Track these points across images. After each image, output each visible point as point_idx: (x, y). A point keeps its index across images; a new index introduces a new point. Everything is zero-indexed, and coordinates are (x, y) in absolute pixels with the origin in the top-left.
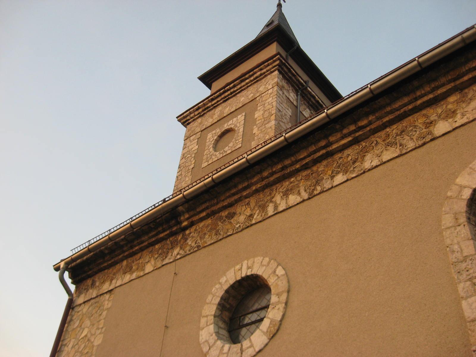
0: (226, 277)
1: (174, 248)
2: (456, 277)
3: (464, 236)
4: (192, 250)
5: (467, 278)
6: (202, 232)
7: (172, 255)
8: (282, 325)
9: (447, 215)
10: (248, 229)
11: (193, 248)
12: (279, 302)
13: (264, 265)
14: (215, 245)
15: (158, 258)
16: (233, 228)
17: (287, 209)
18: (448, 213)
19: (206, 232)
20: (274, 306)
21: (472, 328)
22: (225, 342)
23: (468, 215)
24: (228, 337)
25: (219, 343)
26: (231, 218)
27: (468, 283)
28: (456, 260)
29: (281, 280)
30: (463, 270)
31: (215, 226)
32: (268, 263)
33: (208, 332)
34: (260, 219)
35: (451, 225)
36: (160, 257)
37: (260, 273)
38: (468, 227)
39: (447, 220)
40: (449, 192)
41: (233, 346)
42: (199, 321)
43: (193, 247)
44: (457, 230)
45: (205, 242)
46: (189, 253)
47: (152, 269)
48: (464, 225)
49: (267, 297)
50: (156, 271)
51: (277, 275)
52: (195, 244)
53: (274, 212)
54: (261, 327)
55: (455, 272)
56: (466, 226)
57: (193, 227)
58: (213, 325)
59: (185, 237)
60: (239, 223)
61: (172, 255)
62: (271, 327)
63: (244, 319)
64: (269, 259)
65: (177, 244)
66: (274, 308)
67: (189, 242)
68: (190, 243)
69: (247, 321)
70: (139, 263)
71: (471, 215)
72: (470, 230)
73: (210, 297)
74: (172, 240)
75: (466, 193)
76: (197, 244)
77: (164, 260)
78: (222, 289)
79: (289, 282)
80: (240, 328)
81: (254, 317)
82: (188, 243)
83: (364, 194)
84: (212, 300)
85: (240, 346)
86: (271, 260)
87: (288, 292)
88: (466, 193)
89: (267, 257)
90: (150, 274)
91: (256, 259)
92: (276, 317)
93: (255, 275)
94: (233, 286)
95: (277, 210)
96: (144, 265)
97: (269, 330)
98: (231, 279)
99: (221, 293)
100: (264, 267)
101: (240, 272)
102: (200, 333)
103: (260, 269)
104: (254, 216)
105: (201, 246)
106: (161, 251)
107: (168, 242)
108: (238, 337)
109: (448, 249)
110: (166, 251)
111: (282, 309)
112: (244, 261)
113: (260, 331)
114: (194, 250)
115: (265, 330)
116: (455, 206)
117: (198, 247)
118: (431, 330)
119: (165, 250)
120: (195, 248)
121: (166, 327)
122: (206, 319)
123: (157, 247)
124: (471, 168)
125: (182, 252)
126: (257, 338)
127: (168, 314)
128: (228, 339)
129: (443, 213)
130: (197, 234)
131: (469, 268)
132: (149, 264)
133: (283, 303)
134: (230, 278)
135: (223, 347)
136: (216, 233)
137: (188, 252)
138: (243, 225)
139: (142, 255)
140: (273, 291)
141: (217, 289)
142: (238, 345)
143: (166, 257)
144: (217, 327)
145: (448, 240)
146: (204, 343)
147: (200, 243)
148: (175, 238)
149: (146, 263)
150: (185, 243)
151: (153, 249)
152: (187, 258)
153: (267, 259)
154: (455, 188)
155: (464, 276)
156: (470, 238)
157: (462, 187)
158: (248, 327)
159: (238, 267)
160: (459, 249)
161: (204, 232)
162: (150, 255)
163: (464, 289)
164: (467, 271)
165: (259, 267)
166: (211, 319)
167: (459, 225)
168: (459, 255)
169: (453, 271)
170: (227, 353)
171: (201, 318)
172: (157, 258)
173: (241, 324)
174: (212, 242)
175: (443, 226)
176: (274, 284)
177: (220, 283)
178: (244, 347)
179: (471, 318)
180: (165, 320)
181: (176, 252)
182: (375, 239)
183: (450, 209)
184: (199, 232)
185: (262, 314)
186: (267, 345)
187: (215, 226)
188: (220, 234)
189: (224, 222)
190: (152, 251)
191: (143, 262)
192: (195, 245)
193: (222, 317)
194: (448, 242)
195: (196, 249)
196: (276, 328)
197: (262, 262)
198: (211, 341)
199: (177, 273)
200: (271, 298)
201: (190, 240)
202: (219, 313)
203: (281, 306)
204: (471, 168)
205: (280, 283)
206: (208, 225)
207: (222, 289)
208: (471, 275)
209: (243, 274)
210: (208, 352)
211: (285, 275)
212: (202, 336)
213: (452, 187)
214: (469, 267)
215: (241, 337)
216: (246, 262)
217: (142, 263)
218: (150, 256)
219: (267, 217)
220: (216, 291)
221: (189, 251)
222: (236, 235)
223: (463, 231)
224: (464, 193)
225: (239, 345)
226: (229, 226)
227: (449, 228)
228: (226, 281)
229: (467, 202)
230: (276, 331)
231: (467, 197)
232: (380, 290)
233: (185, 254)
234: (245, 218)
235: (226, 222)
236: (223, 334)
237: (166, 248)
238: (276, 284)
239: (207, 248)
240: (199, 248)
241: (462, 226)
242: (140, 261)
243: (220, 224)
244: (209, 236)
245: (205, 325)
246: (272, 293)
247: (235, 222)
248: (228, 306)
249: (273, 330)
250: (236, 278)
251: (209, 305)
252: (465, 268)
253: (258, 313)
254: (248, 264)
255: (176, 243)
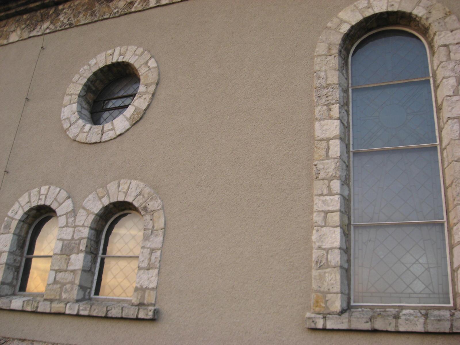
0: (96, 60)
1: (44, 21)
2: (316, 100)
3: (332, 66)
4: (63, 27)
5: (325, 103)
6: (77, 10)
7: (40, 28)
8: (145, 115)
9: (322, 44)
10: (126, 16)
11: (65, 25)
12: (146, 93)
13: (137, 55)
14: (89, 25)
15: (26, 29)
16: (111, 12)
17: (170, 4)
18: (323, 42)
19: (81, 11)
20: (141, 96)
21: (318, 146)
22: (87, 122)
23: (340, 48)
24: (89, 118)
25: (81, 122)
26: (110, 1)
27: (325, 108)
28: (318, 85)
29: (152, 72)
30: (323, 96)
31: (92, 6)
32: (142, 53)
33: (70, 110)
34: (140, 9)
35: (323, 53)
36: (28, 28)
37: (131, 61)
38: (338, 59)
39: (321, 48)
40: (329, 23)
41: (94, 126)
42: (63, 98)
43: (65, 24)
44: (328, 59)
45: (79, 21)
46: (60, 29)
47: (17, 39)
48: (335, 56)
49: (135, 86)
50: (22, 42)
51: (149, 67)
52: (68, 21)
53: (156, 3)
54: (124, 113)
55: (316, 95)
56: (336, 57)
57: (68, 3)
58: (77, 104)
59: (58, 12)
60: (117, 7)
61: (40, 28)
62: (135, 115)
63: (107, 104)
64: (143, 49)
65: (48, 18)
66: (140, 97)
67: (61, 18)
68: (62, 19)
69: (110, 105)
70: (3, 31)
71: (344, 48)
72: (339, 61)
73: (76, 77)
74: (43, 12)
75: (344, 28)
76: (69, 22)
77: (32, 32)
78: (91, 71)
79: (159, 75)
80: (104, 111)
81: (119, 103)
82: (60, 19)
83: (249, 6)
84: (78, 80)
85: (102, 128)
86: (145, 51)
87: (157, 84)
88: (344, 28)
89: (141, 47)
90: (15, 43)
91: (130, 47)
92: (141, 106)
93: (126, 63)
94: (101, 70)
95: (159, 2)
96: (8, 34)
97: (132, 117)
98: (101, 63)
99: (89, 74)
100: (137, 57)
101: (112, 58)
102: (63, 110)
103: (133, 57)
104: (135, 3)
105: (74, 24)
106: (29, 22)
107: (38, 14)
108: (99, 119)
109: (315, 74)
110: (35, 23)
111: (148, 99)
112: (118, 47)
113: (124, 117)
114: (66, 27)
115: (128, 116)
116: (331, 37)
117: (71, 24)
118: (283, 142)
119: (33, 22)
120: (67, 25)
121: (27, 100)
122: (70, 97)
123: (25, 17)
124: (355, 6)
125: (53, 27)
126: (120, 123)
127: (30, 87)
128: (90, 120)
129: (319, 41)
130: (70, 11)
131: (329, 94)
132: (14, 34)
133: (150, 94)
134: (100, 61)
135: (84, 126)
136: (91, 14)
137: (58, 28)
138: (122, 11)
139: (7, 22)
140: (142, 81)
141: (85, 70)
142: (99, 127)
143: (34, 29)
144: (80, 106)
145: (318, 66)
146: (65, 119)
147: (73, 21)
148: (47, 12)
149: (11, 31)
150: (56, 19)
151: (20, 18)
152: (56, 33)
153: (141, 50)
154: (336, 20)
155: (323, 101)
156: (337, 69)
157: (342, 21)
158: (111, 112)
159: (110, 52)
160: (325, 76)
161: (78, 11)
162: (16, 24)
163: (320, 112)
164: (327, 97)
165: (132, 56)
166: (75, 98)
167: (330, 55)
168: (323, 82)
169: (314, 94)
170: (88, 132)
171: (65, 95)
172: (23, 29)
173: (104, 108)
174: (86, 22)
175: (316, 53)
176: (145, 74)
177: (89, 65)
178: (105, 129)
179: (319, 138)
180: (27, 93)
181: (46, 25)
182: (250, 51)
183: (326, 39)
184: (74, 10)
185: (127, 101)
186: (128, 130)
187: (92, 6)
188: (95, 16)
189: (102, 4)
190: (20, 20)
191: (8, 30)
192: (68, 22)
193: (86, 98)
194: (317, 68)
195: (68, 26)
196: (139, 116)
197: (135, 51)
198: (73, 119)
199: (44, 47)
200: (139, 86)
201: (62, 16)
202: (83, 93)
203: (148, 97)
204: (355, 6)
205: (150, 74)
206: (84, 4)
207: (91, 71)
208: (329, 101)
209: (114, 60)
210: (68, 129)
211: (157, 68)
212: (64, 113)
213: (333, 19)
214: (330, 94)
215: (102, 120)
216: (119, 48)
217: (6, 31)
218: (17, 26)
219: (148, 7)
220: (83, 72)
221: (61, 27)
222: (112, 20)
223: (333, 61)
224: (343, 27)
225: (101, 126)
226: (106, 9)
227: (320, 56)
228: (95, 64)
229: (343, 36)
230: (139, 119)
231: (344, 32)
232: (245, 99)
233: (56, 29)
234: (125, 4)
235: (104, 5)
236: (85, 114)
237: (35, 20)
238: (147, 74)
239: (79, 28)
240: (71, 26)
241: (333, 56)
242: (4, 29)
243: (97, 5)
244: (84, 15)
245: (69, 103)
246: (141, 83)
247: (114, 7)
248: (94, 89)
249: (137, 118)
250: (106, 62)
251: (75, 84)
252: (326, 94)
253: (123, 100)
254: (120, 50)
255: (46, 16)
